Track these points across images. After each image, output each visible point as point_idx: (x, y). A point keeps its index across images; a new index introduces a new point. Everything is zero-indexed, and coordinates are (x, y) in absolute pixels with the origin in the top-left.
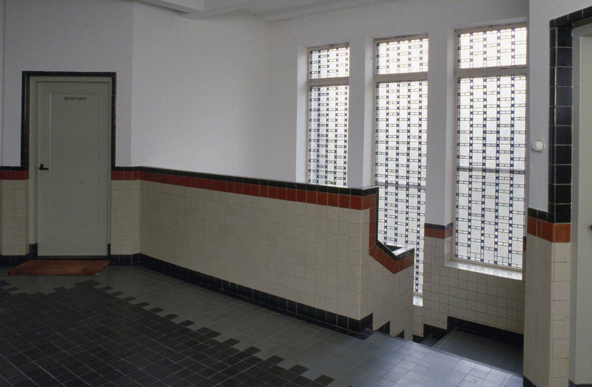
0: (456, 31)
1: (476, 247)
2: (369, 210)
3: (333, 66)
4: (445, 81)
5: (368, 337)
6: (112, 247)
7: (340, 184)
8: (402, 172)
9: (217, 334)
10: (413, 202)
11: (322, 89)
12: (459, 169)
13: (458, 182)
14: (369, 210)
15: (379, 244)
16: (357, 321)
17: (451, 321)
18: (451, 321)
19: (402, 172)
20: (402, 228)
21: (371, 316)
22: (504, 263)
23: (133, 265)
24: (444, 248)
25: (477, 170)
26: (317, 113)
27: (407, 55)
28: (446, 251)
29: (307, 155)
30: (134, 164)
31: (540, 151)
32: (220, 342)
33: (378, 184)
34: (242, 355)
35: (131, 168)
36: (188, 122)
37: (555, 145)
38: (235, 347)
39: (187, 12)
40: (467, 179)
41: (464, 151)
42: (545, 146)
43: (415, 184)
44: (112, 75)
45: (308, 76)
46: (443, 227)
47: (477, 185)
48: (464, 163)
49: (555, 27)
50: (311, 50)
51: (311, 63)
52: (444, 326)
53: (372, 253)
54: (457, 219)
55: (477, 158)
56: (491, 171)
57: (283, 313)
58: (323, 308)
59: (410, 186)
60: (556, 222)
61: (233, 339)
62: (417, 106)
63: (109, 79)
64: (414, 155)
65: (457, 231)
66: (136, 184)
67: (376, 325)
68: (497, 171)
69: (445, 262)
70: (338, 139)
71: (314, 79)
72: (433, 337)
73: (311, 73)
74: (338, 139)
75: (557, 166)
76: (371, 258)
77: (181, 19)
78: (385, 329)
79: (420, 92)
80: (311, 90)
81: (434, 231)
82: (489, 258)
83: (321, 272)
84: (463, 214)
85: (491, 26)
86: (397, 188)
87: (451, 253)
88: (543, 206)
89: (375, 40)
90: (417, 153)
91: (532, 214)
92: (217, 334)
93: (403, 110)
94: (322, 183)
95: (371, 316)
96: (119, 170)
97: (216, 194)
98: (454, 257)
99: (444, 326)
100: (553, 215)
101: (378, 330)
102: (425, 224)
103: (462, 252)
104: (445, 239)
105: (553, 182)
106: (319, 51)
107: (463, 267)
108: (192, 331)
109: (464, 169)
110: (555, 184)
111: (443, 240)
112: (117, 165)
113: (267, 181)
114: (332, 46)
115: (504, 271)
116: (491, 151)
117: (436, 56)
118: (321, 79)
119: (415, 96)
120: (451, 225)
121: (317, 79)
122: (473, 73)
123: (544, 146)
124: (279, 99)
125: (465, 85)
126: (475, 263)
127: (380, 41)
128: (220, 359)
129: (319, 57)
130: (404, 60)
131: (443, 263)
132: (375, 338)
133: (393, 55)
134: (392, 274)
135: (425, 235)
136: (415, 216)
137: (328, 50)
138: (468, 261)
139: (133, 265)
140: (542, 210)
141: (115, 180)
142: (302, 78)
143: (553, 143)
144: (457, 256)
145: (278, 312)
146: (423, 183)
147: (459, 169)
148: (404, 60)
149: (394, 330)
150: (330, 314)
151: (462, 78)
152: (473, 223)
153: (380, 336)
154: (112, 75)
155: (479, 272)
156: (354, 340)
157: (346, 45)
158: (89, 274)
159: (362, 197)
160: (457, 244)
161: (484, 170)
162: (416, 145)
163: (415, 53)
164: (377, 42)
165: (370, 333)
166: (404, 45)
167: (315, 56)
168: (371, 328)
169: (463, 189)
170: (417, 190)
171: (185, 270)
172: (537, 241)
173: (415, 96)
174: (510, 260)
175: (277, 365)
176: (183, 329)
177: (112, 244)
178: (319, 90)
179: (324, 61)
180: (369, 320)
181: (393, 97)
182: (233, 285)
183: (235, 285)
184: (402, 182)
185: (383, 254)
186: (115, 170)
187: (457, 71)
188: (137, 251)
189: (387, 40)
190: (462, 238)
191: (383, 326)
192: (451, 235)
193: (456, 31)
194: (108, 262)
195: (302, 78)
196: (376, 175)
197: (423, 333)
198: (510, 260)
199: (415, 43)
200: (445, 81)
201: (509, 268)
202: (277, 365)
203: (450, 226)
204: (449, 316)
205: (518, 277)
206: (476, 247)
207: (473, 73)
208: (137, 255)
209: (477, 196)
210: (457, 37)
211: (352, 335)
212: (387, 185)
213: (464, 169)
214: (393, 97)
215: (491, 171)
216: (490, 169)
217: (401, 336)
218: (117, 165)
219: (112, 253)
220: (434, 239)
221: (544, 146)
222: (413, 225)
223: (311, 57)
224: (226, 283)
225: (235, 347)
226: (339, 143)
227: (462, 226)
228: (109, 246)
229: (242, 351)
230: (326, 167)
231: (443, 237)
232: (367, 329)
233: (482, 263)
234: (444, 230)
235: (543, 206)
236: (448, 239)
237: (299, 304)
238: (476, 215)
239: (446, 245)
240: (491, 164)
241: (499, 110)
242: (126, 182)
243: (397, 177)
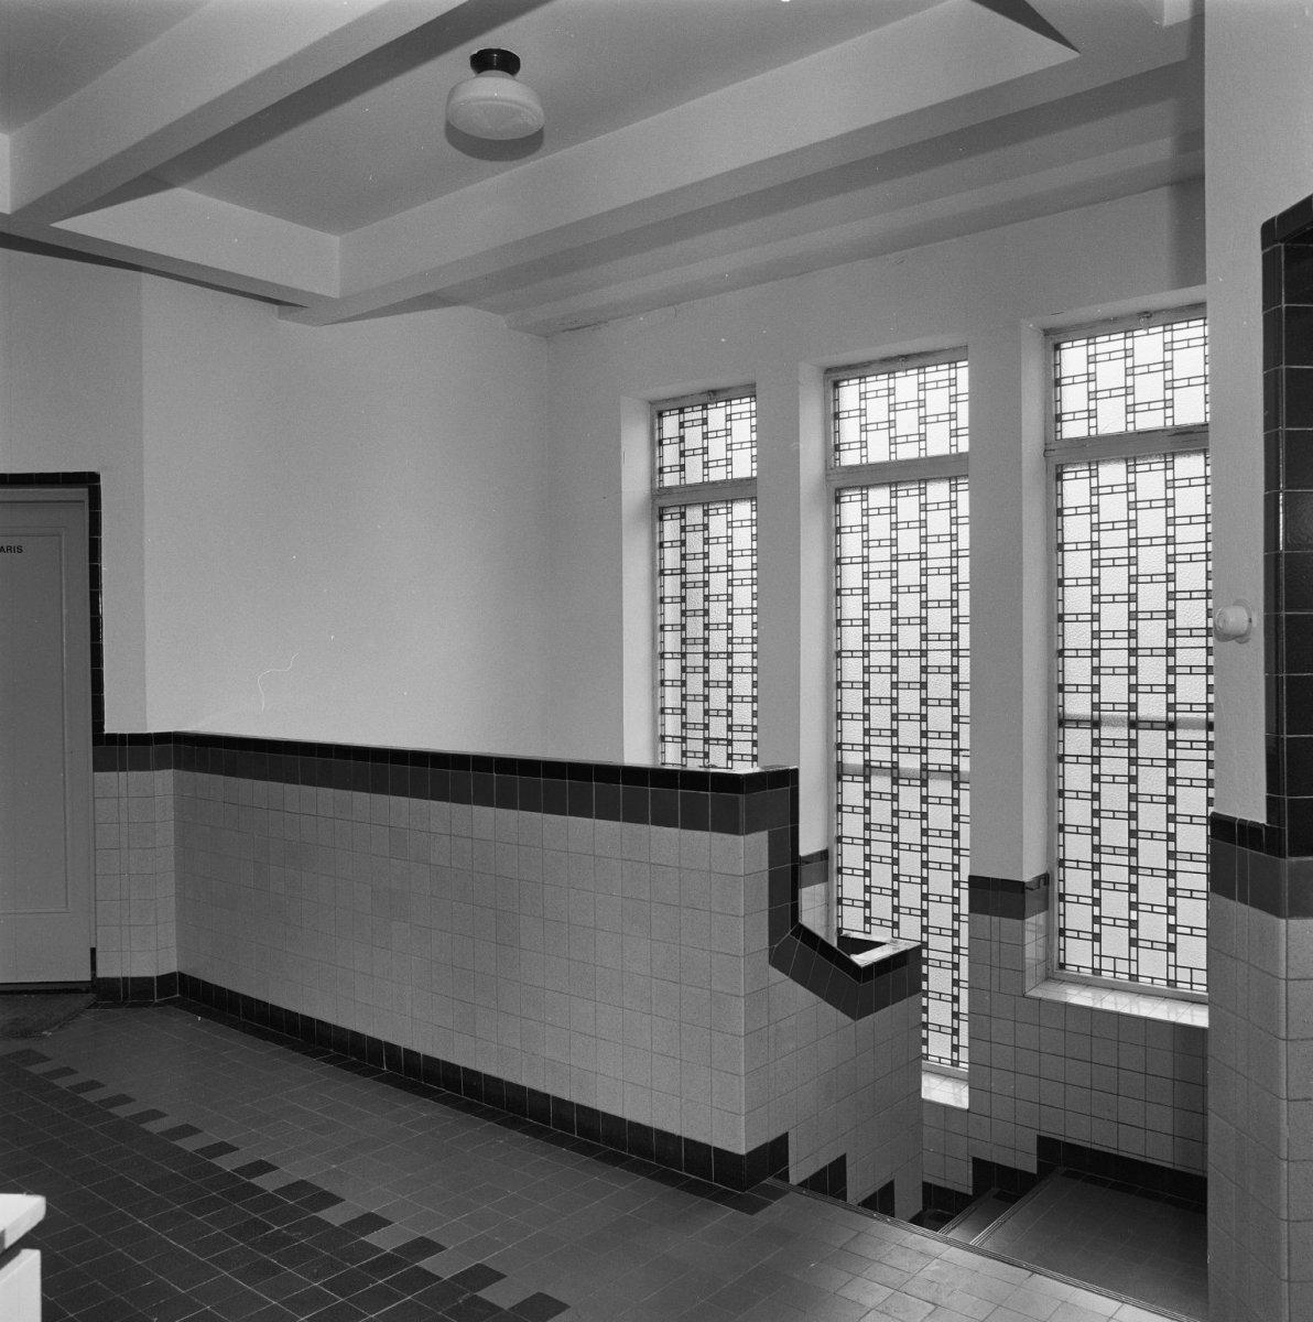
0: (1047, 332)
1: (1115, 941)
2: (766, 832)
3: (717, 449)
4: (1019, 471)
5: (765, 1204)
6: (98, 955)
7: (743, 768)
8: (909, 734)
9: (330, 1199)
10: (940, 817)
11: (689, 513)
12: (1063, 722)
13: (1061, 758)
14: (766, 832)
15: (809, 937)
16: (741, 1157)
17: (1047, 1146)
18: (1047, 1146)
19: (909, 734)
20: (893, 885)
21: (783, 1141)
22: (1195, 987)
23: (158, 1005)
24: (1023, 946)
25: (1114, 723)
26: (677, 580)
27: (912, 410)
28: (1033, 950)
29: (654, 697)
30: (154, 727)
31: (1241, 636)
32: (332, 1226)
33: (845, 770)
34: (388, 1262)
35: (148, 735)
36: (301, 600)
37: (1283, 613)
38: (372, 1238)
39: (294, 302)
40: (1087, 749)
41: (1077, 671)
42: (1254, 619)
43: (943, 768)
44: (90, 481)
45: (652, 480)
46: (1020, 887)
47: (1114, 765)
48: (1078, 705)
49: (1276, 242)
50: (662, 407)
51: (661, 443)
52: (1031, 1165)
53: (778, 959)
54: (1062, 863)
55: (1114, 690)
56: (1152, 725)
57: (537, 1133)
58: (644, 1120)
59: (931, 774)
60: (1291, 855)
61: (373, 1214)
62: (945, 550)
63: (82, 493)
64: (940, 686)
65: (1062, 897)
66: (163, 781)
67: (799, 1171)
68: (1171, 726)
69: (1029, 983)
70: (737, 648)
71: (670, 488)
72: (997, 1196)
73: (661, 470)
74: (737, 648)
75: (1288, 678)
76: (776, 975)
77: (288, 326)
78: (830, 1182)
79: (944, 511)
80: (661, 519)
81: (997, 898)
82: (1152, 965)
83: (647, 1012)
84: (1077, 847)
85: (1146, 312)
86: (895, 781)
87: (1048, 958)
88: (1254, 810)
89: (828, 370)
90: (947, 680)
91: (1222, 828)
92: (330, 1199)
93: (904, 556)
94: (694, 765)
95: (783, 1141)
96: (114, 743)
97: (362, 801)
98: (1056, 970)
99: (1031, 1165)
100: (1281, 832)
101: (800, 1185)
102: (970, 877)
103: (1078, 954)
104: (1030, 920)
105: (1278, 731)
106: (682, 411)
107: (1080, 997)
108: (262, 1190)
109: (1078, 723)
110: (1285, 736)
111: (1019, 922)
112: (108, 729)
113: (468, 756)
114: (714, 396)
115: (1140, 998)
116: (1152, 670)
117: (993, 409)
118: (686, 486)
119: (939, 522)
120: (1045, 879)
121: (676, 487)
122: (1096, 450)
123: (1250, 621)
124: (554, 540)
125: (1075, 490)
126: (1113, 987)
127: (841, 375)
128: (316, 1277)
129: (682, 425)
130: (907, 422)
131: (1023, 987)
132: (777, 1211)
133: (877, 410)
134: (850, 1020)
135: (970, 912)
136: (946, 856)
137: (705, 407)
138: (1094, 980)
139: (158, 1005)
140: (1249, 819)
141: (102, 771)
142: (634, 484)
143: (1277, 608)
144: (1062, 966)
145: (525, 1132)
146: (965, 765)
147: (1063, 722)
148: (907, 422)
149: (859, 1185)
150: (665, 1136)
151: (1068, 464)
152: (1107, 873)
153: (804, 1199)
154: (90, 481)
155: (1126, 1010)
156: (724, 1216)
157: (750, 391)
158: (26, 1034)
159: (742, 798)
160: (1062, 932)
161: (1133, 724)
162: (945, 659)
163: (938, 401)
164: (834, 377)
165: (777, 1194)
166: (906, 384)
167: (670, 424)
168: (785, 1176)
169: (1077, 777)
170: (949, 784)
171: (292, 1016)
172: (1242, 913)
173: (939, 522)
174: (1134, 964)
175: (479, 1294)
176: (238, 1187)
177: (98, 950)
178: (683, 516)
179: (693, 437)
180: (774, 1154)
181: (880, 527)
182: (410, 1054)
183: (417, 1054)
184: (910, 763)
185: (822, 963)
186: (102, 744)
187: (1052, 447)
188: (170, 965)
189: (860, 370)
190: (1077, 917)
191: (823, 1170)
192: (1046, 906)
193: (1047, 332)
194: (91, 997)
195: (634, 484)
196: (839, 746)
197: (971, 1183)
198: (1134, 964)
199: (937, 374)
200: (1019, 471)
201: (1172, 992)
202: (479, 1294)
203: (1042, 882)
204: (1042, 1134)
205: (1199, 1017)
206: (1115, 941)
207: (1096, 450)
208: (171, 976)
209: (1114, 797)
210: (1051, 348)
211: (721, 1197)
212: (867, 773)
213: (1078, 723)
214: (880, 527)
215: (1152, 725)
216: (1150, 718)
217: (882, 1202)
218: (108, 729)
219: (100, 974)
220: (995, 919)
221: (1250, 621)
222: (941, 882)
223: (660, 428)
224: (392, 1048)
225: (372, 1238)
226: (738, 660)
227: (1077, 882)
228: (93, 951)
229: (388, 1251)
230: (706, 727)
231: (1021, 915)
232: (769, 1181)
233: (1133, 985)
234: (1023, 892)
235: (1254, 810)
236: (1035, 921)
237: (581, 1108)
238: (1114, 850)
239: (1029, 937)
240: (1151, 707)
241: (1161, 553)
242: (134, 775)
243: (895, 749)
